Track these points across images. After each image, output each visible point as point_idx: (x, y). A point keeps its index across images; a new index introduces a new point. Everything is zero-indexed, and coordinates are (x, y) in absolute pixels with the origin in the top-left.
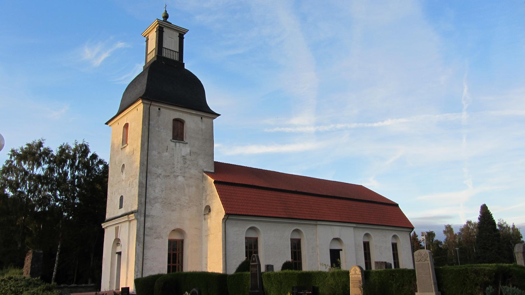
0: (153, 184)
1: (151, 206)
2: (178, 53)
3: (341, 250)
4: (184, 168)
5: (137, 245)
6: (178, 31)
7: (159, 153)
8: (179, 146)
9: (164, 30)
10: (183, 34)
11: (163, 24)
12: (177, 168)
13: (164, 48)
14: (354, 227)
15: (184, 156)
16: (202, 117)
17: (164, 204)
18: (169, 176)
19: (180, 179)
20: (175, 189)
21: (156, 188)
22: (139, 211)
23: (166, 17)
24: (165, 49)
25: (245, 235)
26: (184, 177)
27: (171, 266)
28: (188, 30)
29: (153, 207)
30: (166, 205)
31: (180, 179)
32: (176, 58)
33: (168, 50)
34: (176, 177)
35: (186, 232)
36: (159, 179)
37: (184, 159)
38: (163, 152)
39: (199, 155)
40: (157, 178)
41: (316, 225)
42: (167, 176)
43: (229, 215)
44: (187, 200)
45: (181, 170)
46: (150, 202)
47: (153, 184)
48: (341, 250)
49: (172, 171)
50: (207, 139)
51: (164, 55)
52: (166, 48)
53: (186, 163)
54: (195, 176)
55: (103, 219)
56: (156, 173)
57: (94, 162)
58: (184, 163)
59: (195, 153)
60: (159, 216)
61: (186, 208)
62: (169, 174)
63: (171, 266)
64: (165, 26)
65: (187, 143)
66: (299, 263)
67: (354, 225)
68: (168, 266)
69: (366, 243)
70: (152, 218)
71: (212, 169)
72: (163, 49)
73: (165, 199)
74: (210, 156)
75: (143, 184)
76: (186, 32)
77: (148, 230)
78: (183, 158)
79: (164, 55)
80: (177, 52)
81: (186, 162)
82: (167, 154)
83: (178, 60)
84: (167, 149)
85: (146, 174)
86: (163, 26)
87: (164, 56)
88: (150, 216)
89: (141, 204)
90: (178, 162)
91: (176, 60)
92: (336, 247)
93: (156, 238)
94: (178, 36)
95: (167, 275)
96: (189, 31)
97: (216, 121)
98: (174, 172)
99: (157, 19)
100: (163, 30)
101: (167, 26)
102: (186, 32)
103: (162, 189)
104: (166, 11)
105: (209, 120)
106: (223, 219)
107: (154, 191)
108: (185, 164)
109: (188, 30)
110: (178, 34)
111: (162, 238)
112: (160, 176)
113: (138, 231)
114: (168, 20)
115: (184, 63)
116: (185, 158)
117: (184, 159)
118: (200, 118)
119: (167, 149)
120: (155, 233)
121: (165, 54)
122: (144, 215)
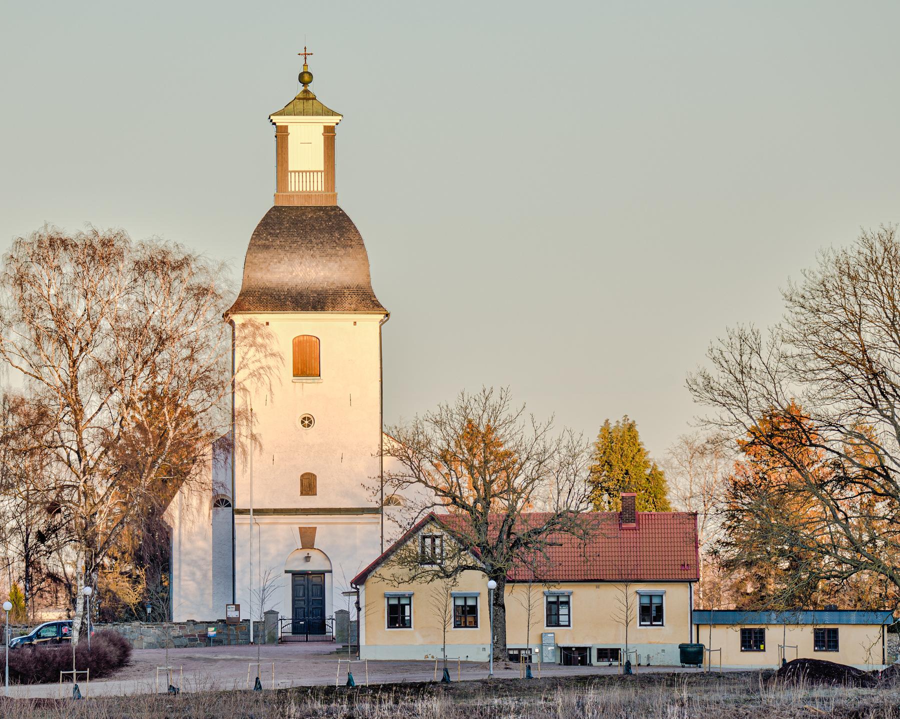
2: (323, 173)
13: (291, 172)
52: (295, 172)
72: (289, 173)
80: (321, 172)
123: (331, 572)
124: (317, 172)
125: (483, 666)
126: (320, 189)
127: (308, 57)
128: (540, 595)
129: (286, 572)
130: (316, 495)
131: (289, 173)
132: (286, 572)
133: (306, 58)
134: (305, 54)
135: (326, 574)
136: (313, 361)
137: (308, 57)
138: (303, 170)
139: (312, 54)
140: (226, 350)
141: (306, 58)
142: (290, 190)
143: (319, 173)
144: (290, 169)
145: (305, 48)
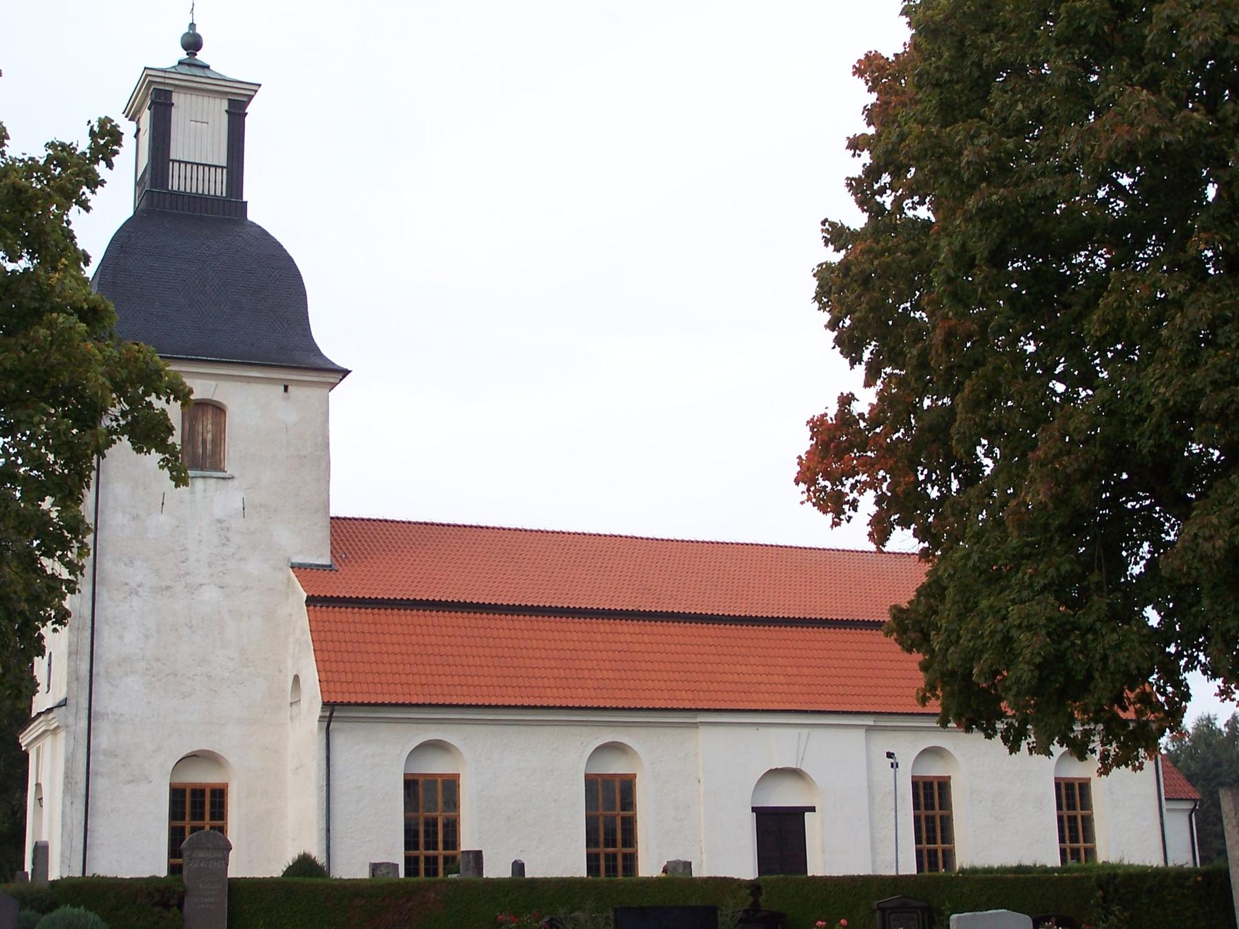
0: (115, 617)
1: (112, 685)
2: (225, 171)
3: (812, 809)
4: (224, 559)
5: (68, 803)
6: (226, 93)
7: (135, 518)
8: (205, 491)
9: (173, 102)
10: (246, 99)
11: (167, 81)
12: (198, 560)
13: (174, 161)
14: (869, 729)
15: (220, 521)
16: (286, 384)
17: (153, 676)
18: (168, 588)
19: (210, 594)
20: (191, 627)
21: (125, 628)
22: (71, 702)
23: (192, 43)
24: (176, 165)
25: (405, 770)
26: (222, 588)
27: (602, 845)
28: (260, 85)
29: (117, 686)
30: (160, 680)
31: (210, 594)
32: (217, 186)
33: (195, 167)
34: (193, 589)
35: (230, 761)
36: (135, 598)
37: (222, 529)
38: (149, 514)
39: (275, 511)
40: (129, 598)
41: (696, 725)
42: (162, 589)
43: (336, 707)
44: (233, 659)
45: (210, 566)
46: (106, 672)
47: (115, 617)
48: (812, 809)
49: (182, 572)
50: (305, 456)
51: (175, 184)
52: (180, 162)
53: (229, 540)
54: (260, 581)
55: (24, 719)
56: (125, 581)
57: (1095, 314)
58: (222, 542)
59: (261, 506)
60: (137, 716)
61: (229, 686)
62: (169, 583)
63: (602, 845)
64: (176, 86)
65: (233, 478)
66: (625, 856)
67: (869, 721)
68: (406, 858)
69: (931, 784)
70: (116, 721)
71: (321, 556)
72: (171, 163)
73: (158, 660)
74: (316, 512)
75: (84, 618)
76: (253, 93)
77: (102, 758)
78: (219, 525)
79: (175, 184)
80: (222, 167)
81: (228, 540)
82: (163, 518)
83: (224, 195)
84: (163, 504)
85: (91, 588)
86: (167, 88)
87: (176, 188)
88: (107, 714)
89: (77, 679)
90: (200, 541)
91: (219, 193)
92: (784, 796)
93: (129, 782)
94: (226, 111)
95: (369, 880)
96: (260, 90)
97: (340, 396)
98: (188, 574)
99: (145, 68)
100: (171, 98)
101: (182, 83)
102: (253, 93)
103: (148, 630)
104: (192, 25)
105: (315, 393)
106: (321, 718)
107: (121, 638)
108: (223, 545)
109: (260, 85)
110: (225, 105)
111: (150, 782)
112: (140, 589)
113: (70, 760)
114: (201, 56)
115: (246, 203)
116: (224, 525)
117: (222, 529)
118: (283, 388)
119: (163, 504)
120: (124, 766)
121: (178, 181)
122: (87, 712)
131: (171, 163)
142: (170, 188)
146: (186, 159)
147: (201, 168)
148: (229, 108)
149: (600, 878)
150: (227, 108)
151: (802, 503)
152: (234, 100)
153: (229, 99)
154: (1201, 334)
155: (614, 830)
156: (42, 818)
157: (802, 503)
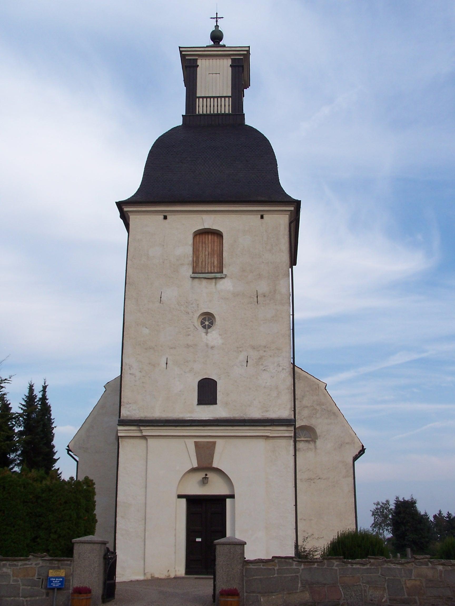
2: (230, 99)
13: (199, 97)
52: (203, 98)
72: (198, 99)
80: (229, 97)
83: (230, 112)
104: (217, 26)
123: (232, 496)
124: (225, 97)
125: (125, 208)
126: (227, 112)
127: (219, 20)
128: (453, 515)
129: (180, 496)
130: (216, 404)
131: (198, 99)
132: (180, 496)
133: (217, 21)
134: (217, 18)
135: (228, 500)
136: (57, 585)
137: (219, 20)
138: (218, 95)
139: (222, 18)
140: (299, 413)
141: (217, 21)
142: (197, 113)
143: (227, 99)
144: (198, 96)
145: (217, 14)
146: (203, 95)
147: (212, 99)
148: (232, 64)
149: (20, 583)
150: (230, 64)
151: (371, 511)
152: (194, 59)
153: (231, 59)
154: (13, 448)
155: (50, 588)
156: (199, 442)
157: (371, 511)
